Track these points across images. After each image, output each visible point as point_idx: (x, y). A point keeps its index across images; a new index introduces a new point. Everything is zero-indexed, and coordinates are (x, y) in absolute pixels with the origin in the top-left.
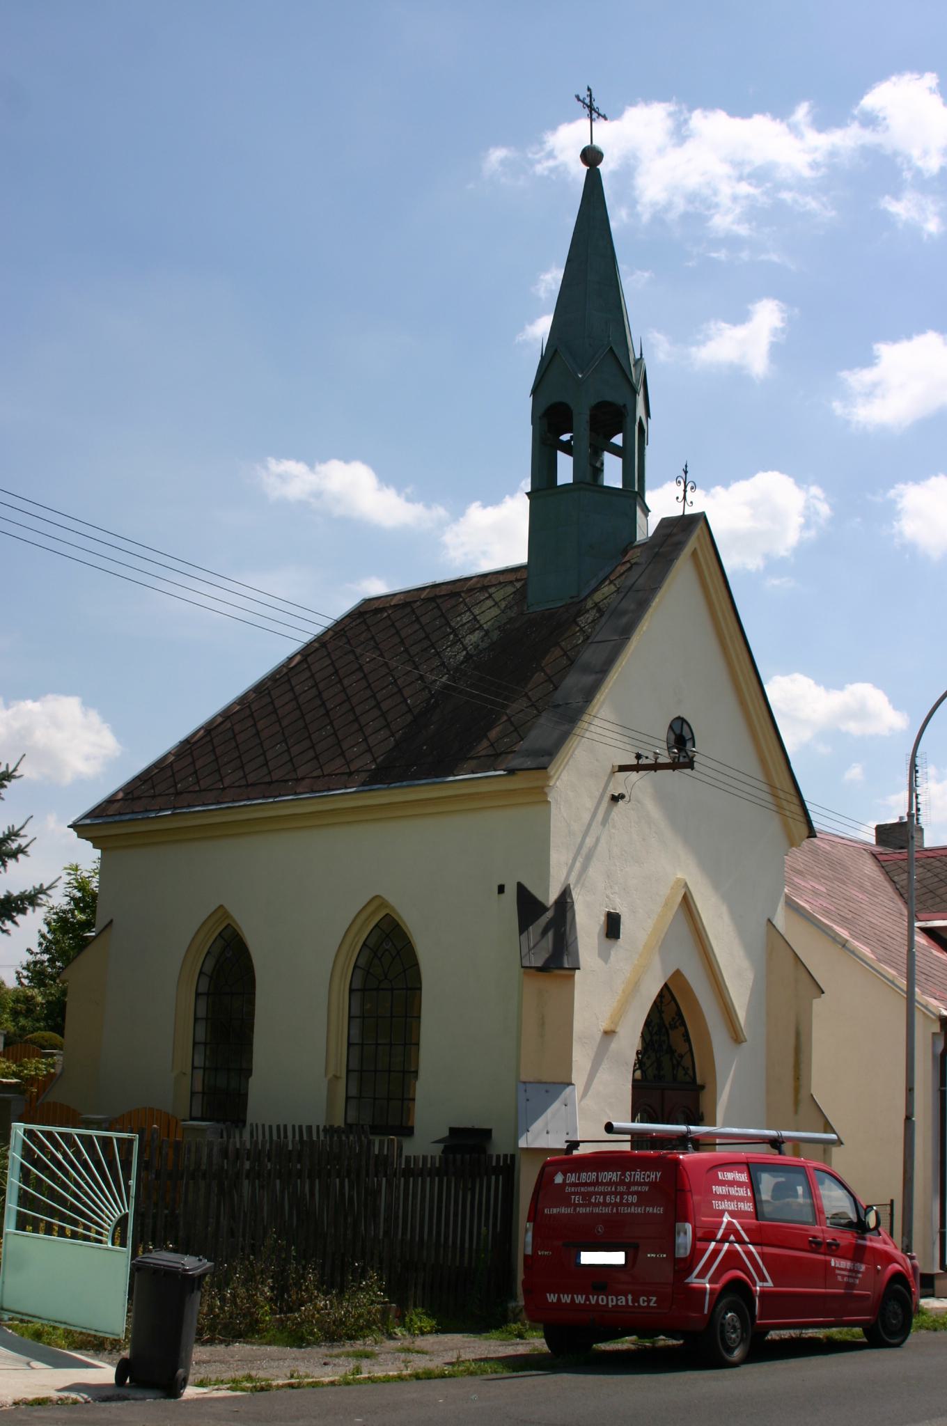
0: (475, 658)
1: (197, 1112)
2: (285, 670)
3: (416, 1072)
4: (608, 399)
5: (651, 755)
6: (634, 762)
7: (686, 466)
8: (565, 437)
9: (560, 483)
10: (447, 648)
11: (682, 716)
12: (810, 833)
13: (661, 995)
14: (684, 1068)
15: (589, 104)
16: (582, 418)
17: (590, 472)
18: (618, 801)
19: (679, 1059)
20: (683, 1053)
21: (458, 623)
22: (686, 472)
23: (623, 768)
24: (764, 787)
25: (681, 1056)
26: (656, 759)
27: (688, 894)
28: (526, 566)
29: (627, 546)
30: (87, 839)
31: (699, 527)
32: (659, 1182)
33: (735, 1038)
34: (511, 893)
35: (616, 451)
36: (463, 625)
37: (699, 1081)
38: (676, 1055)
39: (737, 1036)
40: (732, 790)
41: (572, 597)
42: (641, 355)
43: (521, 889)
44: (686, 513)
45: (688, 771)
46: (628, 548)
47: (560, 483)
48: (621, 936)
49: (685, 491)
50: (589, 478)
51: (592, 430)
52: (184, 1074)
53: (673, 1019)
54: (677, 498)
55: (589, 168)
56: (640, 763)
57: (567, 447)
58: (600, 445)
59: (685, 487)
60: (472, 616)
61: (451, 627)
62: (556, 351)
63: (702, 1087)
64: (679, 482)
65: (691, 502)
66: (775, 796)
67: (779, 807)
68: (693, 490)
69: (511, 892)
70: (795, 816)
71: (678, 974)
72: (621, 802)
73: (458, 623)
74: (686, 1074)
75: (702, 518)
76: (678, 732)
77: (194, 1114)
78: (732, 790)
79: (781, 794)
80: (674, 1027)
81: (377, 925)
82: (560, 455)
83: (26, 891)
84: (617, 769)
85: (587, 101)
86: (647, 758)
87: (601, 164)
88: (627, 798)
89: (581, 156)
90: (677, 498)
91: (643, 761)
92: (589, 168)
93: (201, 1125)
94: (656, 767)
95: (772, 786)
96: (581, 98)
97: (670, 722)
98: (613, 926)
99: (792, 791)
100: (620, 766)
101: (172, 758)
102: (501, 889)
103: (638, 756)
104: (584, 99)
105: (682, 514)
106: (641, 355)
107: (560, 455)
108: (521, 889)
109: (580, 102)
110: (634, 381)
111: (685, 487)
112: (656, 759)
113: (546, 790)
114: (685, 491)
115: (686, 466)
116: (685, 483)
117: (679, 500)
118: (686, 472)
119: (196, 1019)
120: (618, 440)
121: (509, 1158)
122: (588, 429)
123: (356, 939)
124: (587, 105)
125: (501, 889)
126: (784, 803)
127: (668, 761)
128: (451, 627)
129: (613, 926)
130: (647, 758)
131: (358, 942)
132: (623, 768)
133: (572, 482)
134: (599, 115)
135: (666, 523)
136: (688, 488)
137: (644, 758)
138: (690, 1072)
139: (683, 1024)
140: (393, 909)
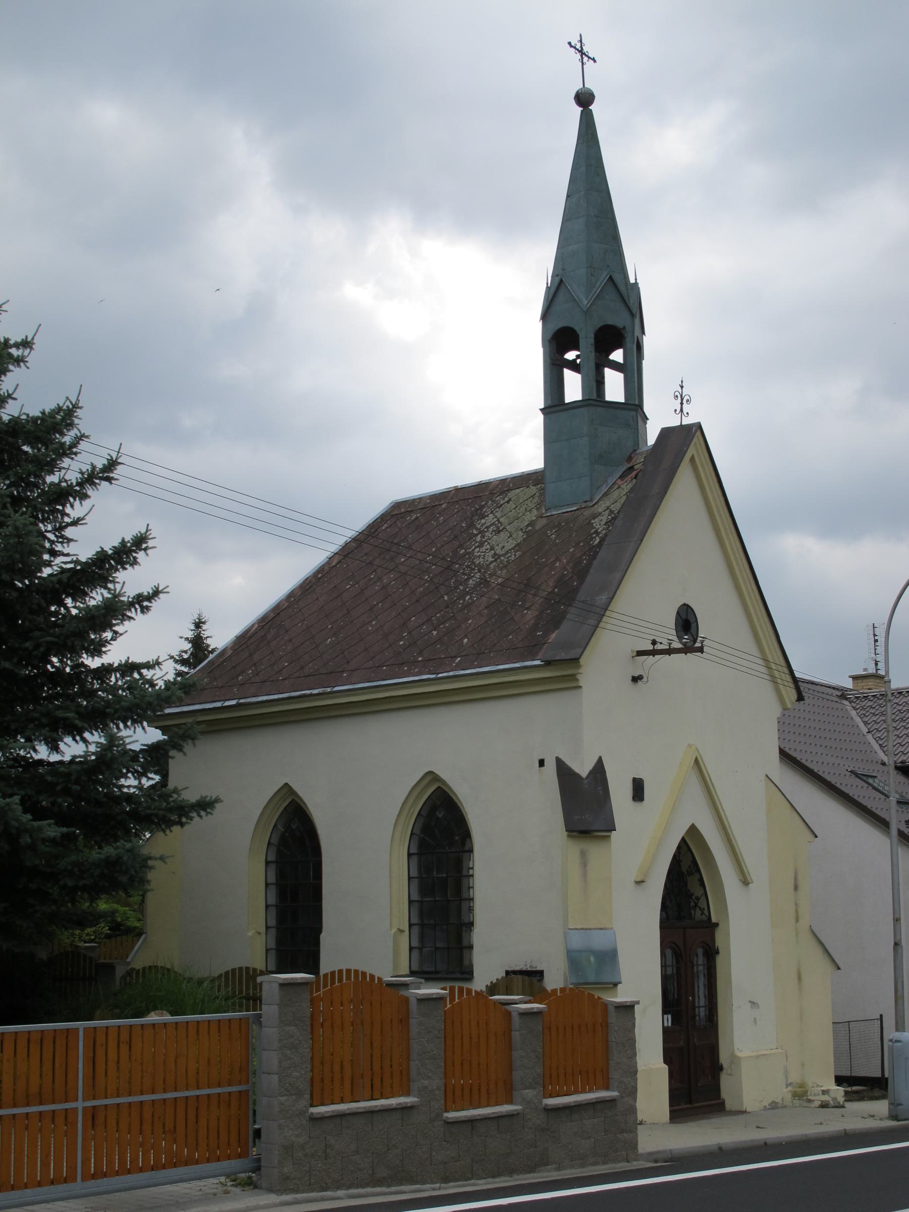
0: (502, 558)
1: (272, 967)
2: (326, 568)
3: (472, 924)
4: (610, 322)
5: (665, 642)
6: (651, 647)
7: (682, 382)
8: (571, 355)
9: (567, 400)
10: (475, 548)
11: (686, 603)
12: (798, 697)
13: (679, 847)
14: (700, 908)
15: (584, 56)
16: (587, 338)
17: (595, 385)
18: (637, 682)
19: (696, 901)
20: (699, 896)
21: (483, 525)
22: (682, 387)
23: (640, 653)
24: (761, 662)
25: (698, 899)
26: (670, 644)
27: (699, 758)
28: (542, 471)
29: (632, 454)
30: (156, 728)
31: (695, 440)
32: (378, 983)
33: (743, 880)
34: (551, 767)
35: (615, 366)
36: (488, 527)
37: (714, 920)
38: (694, 897)
39: (745, 879)
40: (728, 664)
41: (586, 502)
42: (636, 279)
43: (560, 763)
44: (683, 424)
45: (699, 654)
46: (633, 455)
47: (567, 400)
48: (538, 762)
49: (682, 404)
50: (594, 396)
51: (596, 351)
52: (259, 933)
53: (690, 866)
54: (676, 410)
55: (582, 109)
56: (655, 648)
57: (573, 366)
58: (602, 362)
59: (682, 399)
60: (496, 519)
61: (477, 529)
62: (561, 281)
63: (717, 925)
64: (677, 396)
65: (687, 413)
66: (769, 668)
67: (772, 676)
68: (688, 403)
69: (551, 765)
70: (786, 684)
71: (693, 830)
72: (640, 682)
73: (483, 525)
74: (703, 913)
75: (699, 426)
76: (684, 617)
77: (269, 969)
78: (728, 664)
79: (773, 666)
80: (690, 873)
81: (429, 797)
82: (567, 373)
83: (206, 797)
84: (635, 654)
85: (585, 59)
86: (661, 643)
87: (592, 106)
88: (645, 679)
89: (574, 98)
90: (676, 410)
91: (659, 647)
92: (582, 109)
93: (296, 979)
94: (669, 651)
95: (766, 660)
96: (573, 44)
97: (677, 610)
98: (638, 790)
99: (783, 662)
100: (638, 652)
101: (230, 652)
102: (542, 763)
103: (654, 642)
104: (588, 61)
105: (679, 424)
106: (636, 279)
107: (567, 373)
108: (560, 763)
109: (572, 49)
110: (631, 304)
111: (682, 399)
112: (670, 644)
113: (578, 677)
114: (682, 404)
115: (682, 382)
116: (681, 396)
117: (677, 412)
118: (682, 387)
119: (267, 885)
120: (617, 356)
121: (237, 970)
122: (593, 350)
123: (412, 810)
124: (578, 50)
125: (542, 763)
126: (776, 672)
127: (680, 646)
128: (477, 529)
129: (638, 790)
130: (661, 643)
131: (414, 811)
132: (640, 653)
133: (580, 398)
134: (589, 58)
135: (666, 433)
136: (684, 401)
137: (659, 644)
138: (706, 912)
139: (699, 871)
140: (444, 782)
